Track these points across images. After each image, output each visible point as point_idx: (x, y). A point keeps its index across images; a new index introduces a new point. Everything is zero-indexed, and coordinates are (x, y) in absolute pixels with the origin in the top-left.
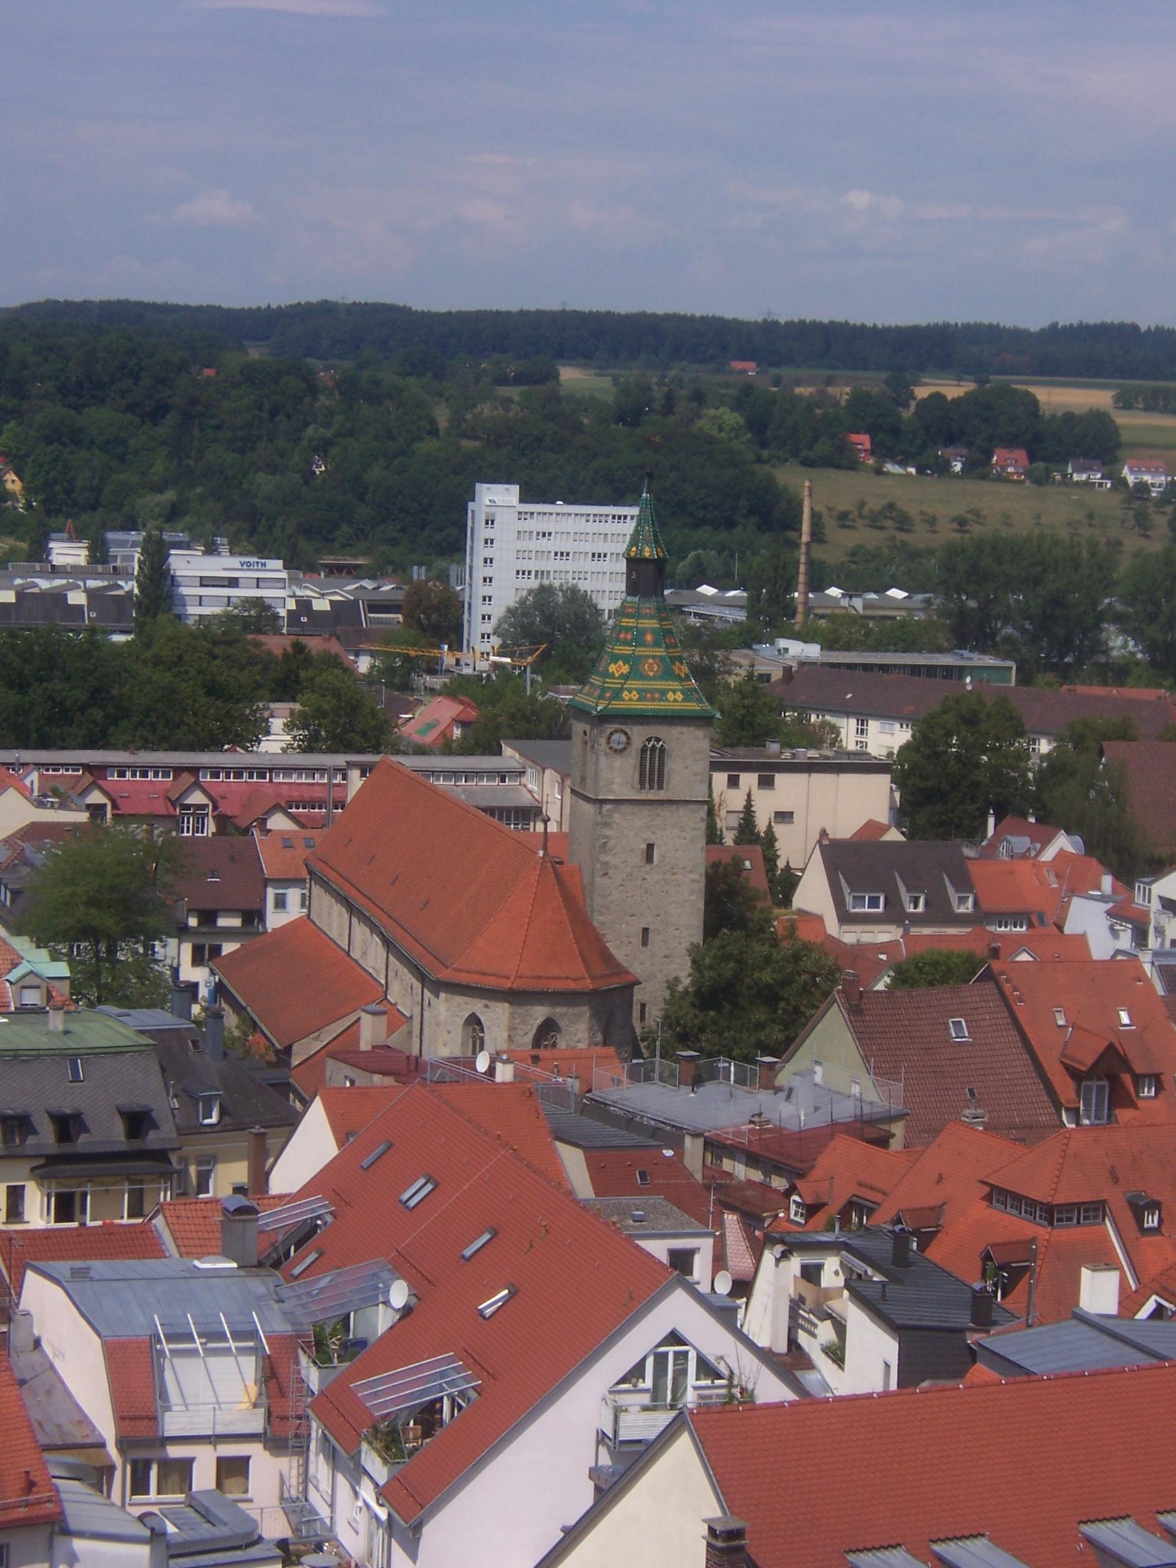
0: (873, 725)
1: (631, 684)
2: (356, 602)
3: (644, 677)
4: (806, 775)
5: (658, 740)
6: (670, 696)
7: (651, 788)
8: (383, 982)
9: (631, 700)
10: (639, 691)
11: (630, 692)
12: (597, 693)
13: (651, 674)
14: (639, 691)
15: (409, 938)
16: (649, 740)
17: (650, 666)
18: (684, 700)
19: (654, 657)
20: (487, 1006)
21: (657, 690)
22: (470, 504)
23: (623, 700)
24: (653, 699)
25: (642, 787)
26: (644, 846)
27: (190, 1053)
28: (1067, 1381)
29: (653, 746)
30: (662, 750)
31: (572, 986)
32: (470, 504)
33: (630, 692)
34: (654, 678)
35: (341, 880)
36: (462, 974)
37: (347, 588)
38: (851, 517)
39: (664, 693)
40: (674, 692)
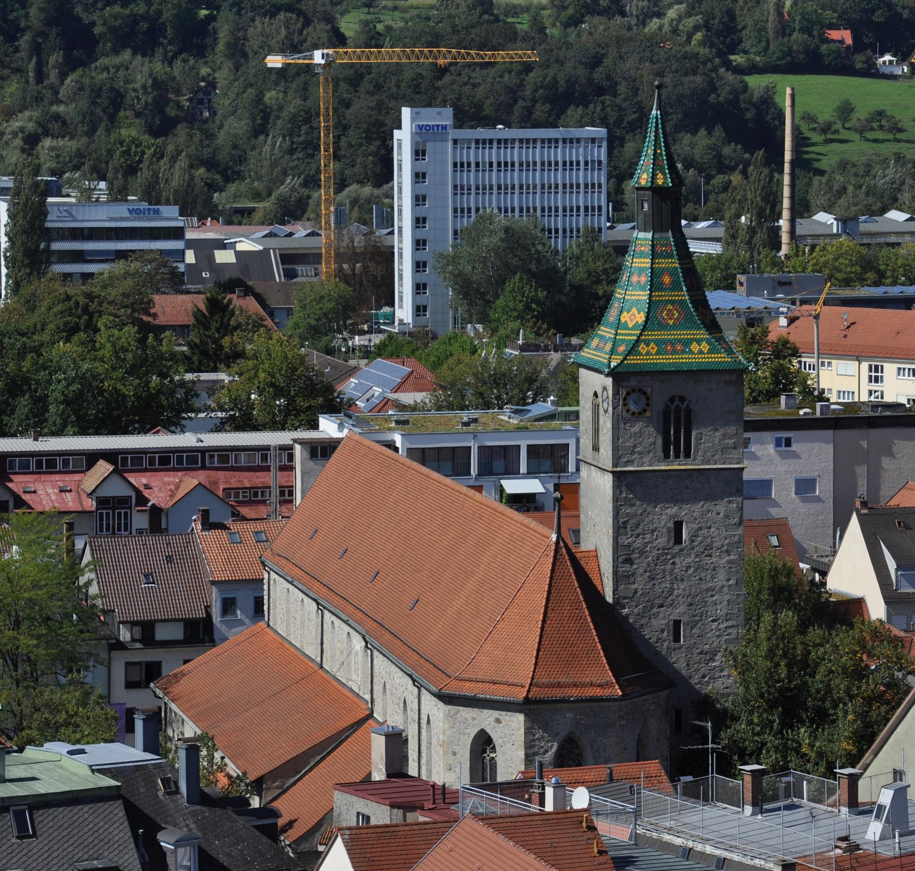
0: (890, 369)
1: (649, 335)
2: (266, 251)
3: (664, 326)
4: (832, 431)
5: (682, 399)
6: (695, 347)
7: (677, 456)
8: (367, 697)
9: (648, 353)
10: (658, 343)
11: (648, 345)
12: (609, 346)
13: (671, 322)
14: (658, 343)
15: (399, 644)
16: (672, 400)
17: (670, 315)
18: (710, 352)
19: (672, 302)
20: (498, 721)
21: (679, 341)
22: (395, 132)
23: (640, 354)
24: (674, 352)
25: (667, 456)
26: (671, 525)
27: (160, 793)
28: (527, 818)
29: (677, 406)
30: (689, 412)
31: (598, 692)
32: (395, 132)
33: (648, 345)
34: (675, 327)
35: (308, 578)
36: (468, 684)
37: (254, 236)
38: (834, 128)
39: (687, 343)
40: (699, 341)
